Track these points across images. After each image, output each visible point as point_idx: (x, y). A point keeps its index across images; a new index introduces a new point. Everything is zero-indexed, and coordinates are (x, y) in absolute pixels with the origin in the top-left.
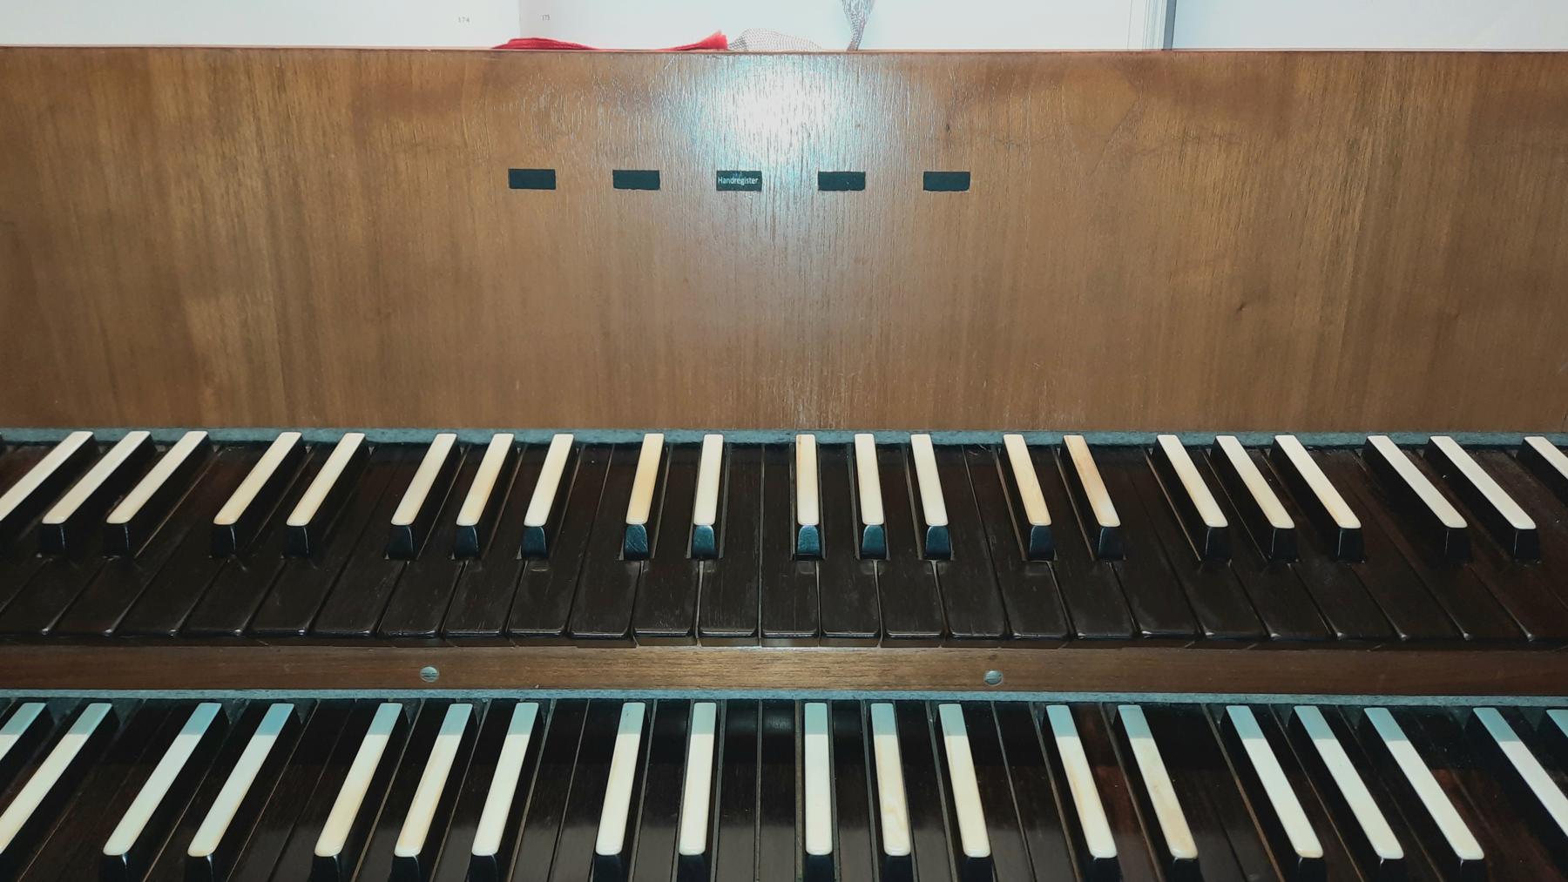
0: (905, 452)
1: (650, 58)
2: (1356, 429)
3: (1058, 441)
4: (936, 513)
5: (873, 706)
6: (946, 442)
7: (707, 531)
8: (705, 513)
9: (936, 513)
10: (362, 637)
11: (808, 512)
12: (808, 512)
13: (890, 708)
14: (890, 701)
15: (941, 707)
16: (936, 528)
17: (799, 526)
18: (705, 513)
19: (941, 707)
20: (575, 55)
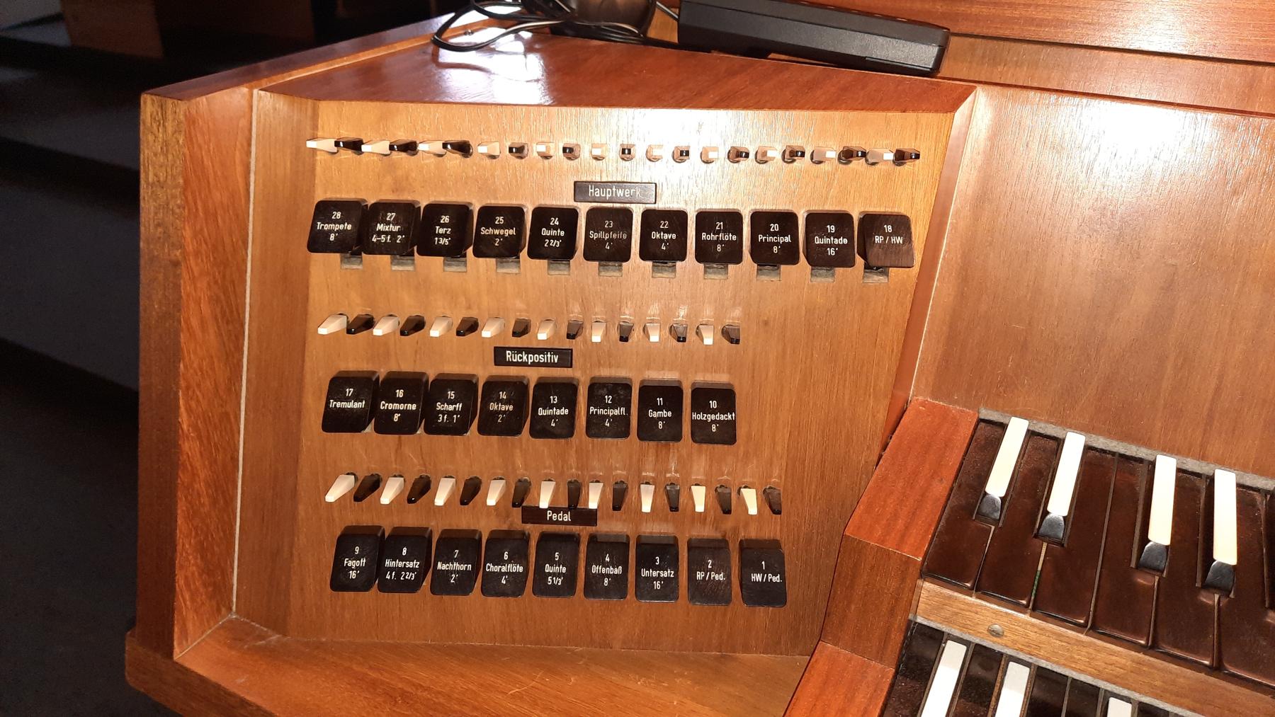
0: (1142, 469)
1: (509, 109)
2: (1202, 457)
3: (1151, 458)
4: (1226, 550)
5: (1011, 664)
6: (1248, 483)
7: (993, 500)
8: (1060, 503)
9: (1226, 550)
10: (1019, 604)
11: (1161, 531)
12: (1161, 531)
13: (962, 649)
14: (965, 642)
15: (1112, 701)
16: (1222, 565)
17: (1046, 513)
18: (1060, 503)
19: (1112, 701)
20: (492, 112)
